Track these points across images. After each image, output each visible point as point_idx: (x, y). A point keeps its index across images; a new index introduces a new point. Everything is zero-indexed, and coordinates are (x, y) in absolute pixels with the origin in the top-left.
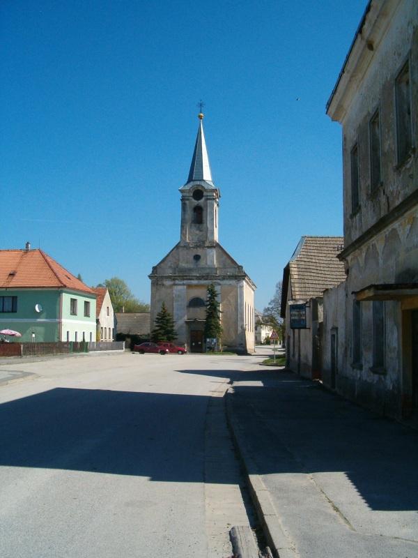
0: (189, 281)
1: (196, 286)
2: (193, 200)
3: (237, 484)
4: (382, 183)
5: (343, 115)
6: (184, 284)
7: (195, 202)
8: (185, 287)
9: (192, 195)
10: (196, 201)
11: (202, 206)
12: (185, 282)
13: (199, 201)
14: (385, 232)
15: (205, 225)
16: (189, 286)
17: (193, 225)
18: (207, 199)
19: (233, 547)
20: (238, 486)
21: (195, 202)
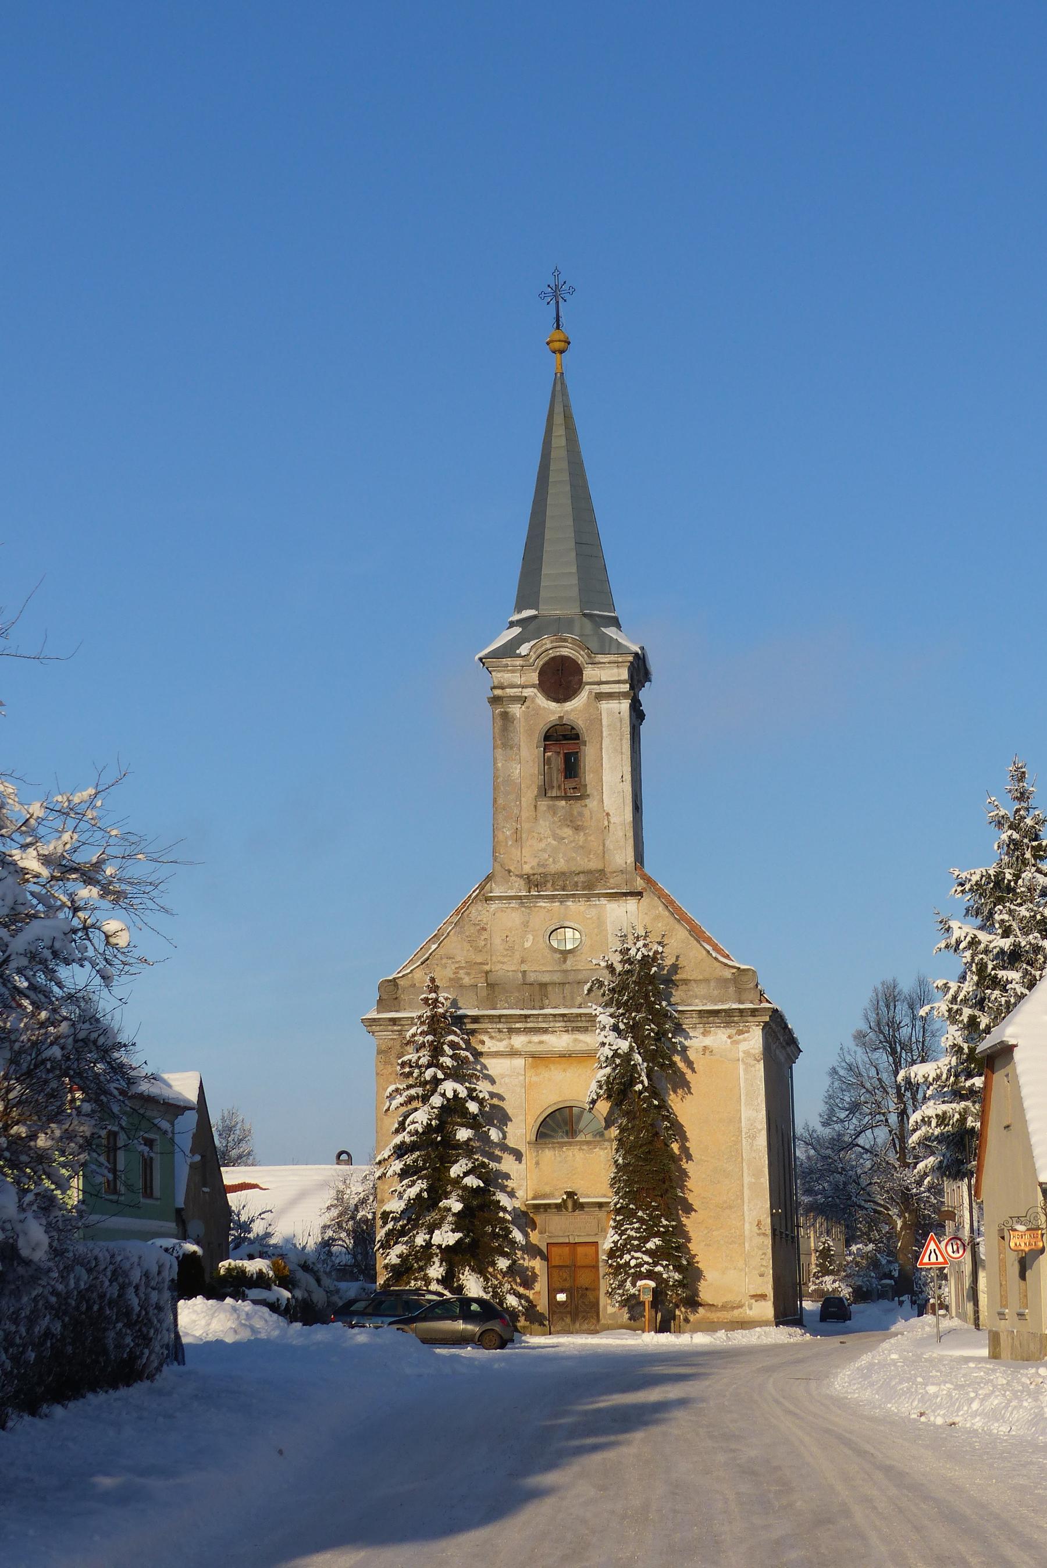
0: (536, 1038)
1: (566, 1057)
2: (542, 701)
3: (190, 1345)
4: (954, 1022)
5: (847, 1435)
6: (513, 1053)
7: (551, 710)
8: (519, 1062)
9: (534, 677)
10: (553, 705)
11: (581, 724)
12: (519, 1041)
13: (569, 706)
14: (995, 1415)
15: (592, 804)
16: (538, 1059)
17: (543, 804)
18: (600, 697)
19: (436, 1339)
20: (181, 1303)
21: (551, 710)
